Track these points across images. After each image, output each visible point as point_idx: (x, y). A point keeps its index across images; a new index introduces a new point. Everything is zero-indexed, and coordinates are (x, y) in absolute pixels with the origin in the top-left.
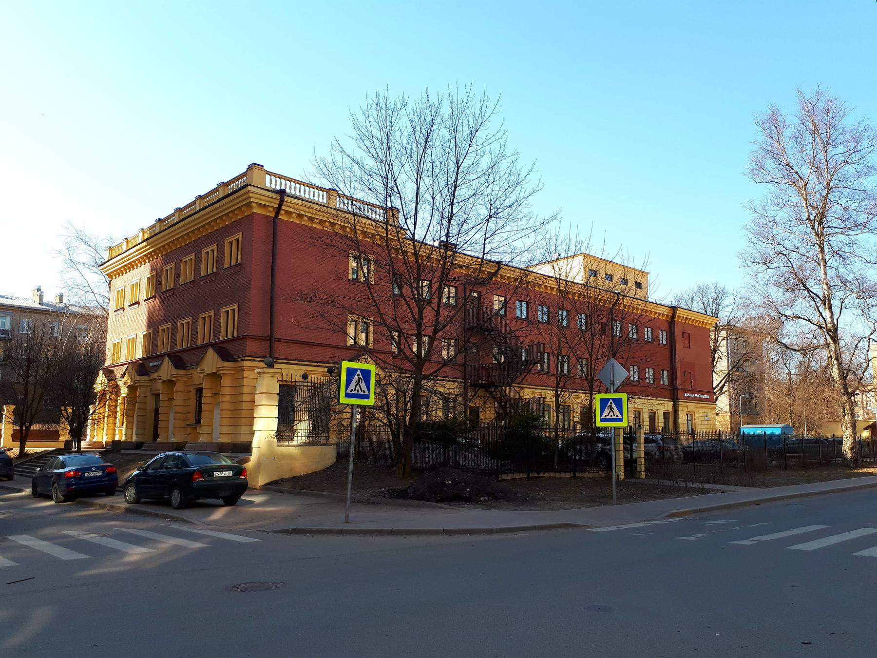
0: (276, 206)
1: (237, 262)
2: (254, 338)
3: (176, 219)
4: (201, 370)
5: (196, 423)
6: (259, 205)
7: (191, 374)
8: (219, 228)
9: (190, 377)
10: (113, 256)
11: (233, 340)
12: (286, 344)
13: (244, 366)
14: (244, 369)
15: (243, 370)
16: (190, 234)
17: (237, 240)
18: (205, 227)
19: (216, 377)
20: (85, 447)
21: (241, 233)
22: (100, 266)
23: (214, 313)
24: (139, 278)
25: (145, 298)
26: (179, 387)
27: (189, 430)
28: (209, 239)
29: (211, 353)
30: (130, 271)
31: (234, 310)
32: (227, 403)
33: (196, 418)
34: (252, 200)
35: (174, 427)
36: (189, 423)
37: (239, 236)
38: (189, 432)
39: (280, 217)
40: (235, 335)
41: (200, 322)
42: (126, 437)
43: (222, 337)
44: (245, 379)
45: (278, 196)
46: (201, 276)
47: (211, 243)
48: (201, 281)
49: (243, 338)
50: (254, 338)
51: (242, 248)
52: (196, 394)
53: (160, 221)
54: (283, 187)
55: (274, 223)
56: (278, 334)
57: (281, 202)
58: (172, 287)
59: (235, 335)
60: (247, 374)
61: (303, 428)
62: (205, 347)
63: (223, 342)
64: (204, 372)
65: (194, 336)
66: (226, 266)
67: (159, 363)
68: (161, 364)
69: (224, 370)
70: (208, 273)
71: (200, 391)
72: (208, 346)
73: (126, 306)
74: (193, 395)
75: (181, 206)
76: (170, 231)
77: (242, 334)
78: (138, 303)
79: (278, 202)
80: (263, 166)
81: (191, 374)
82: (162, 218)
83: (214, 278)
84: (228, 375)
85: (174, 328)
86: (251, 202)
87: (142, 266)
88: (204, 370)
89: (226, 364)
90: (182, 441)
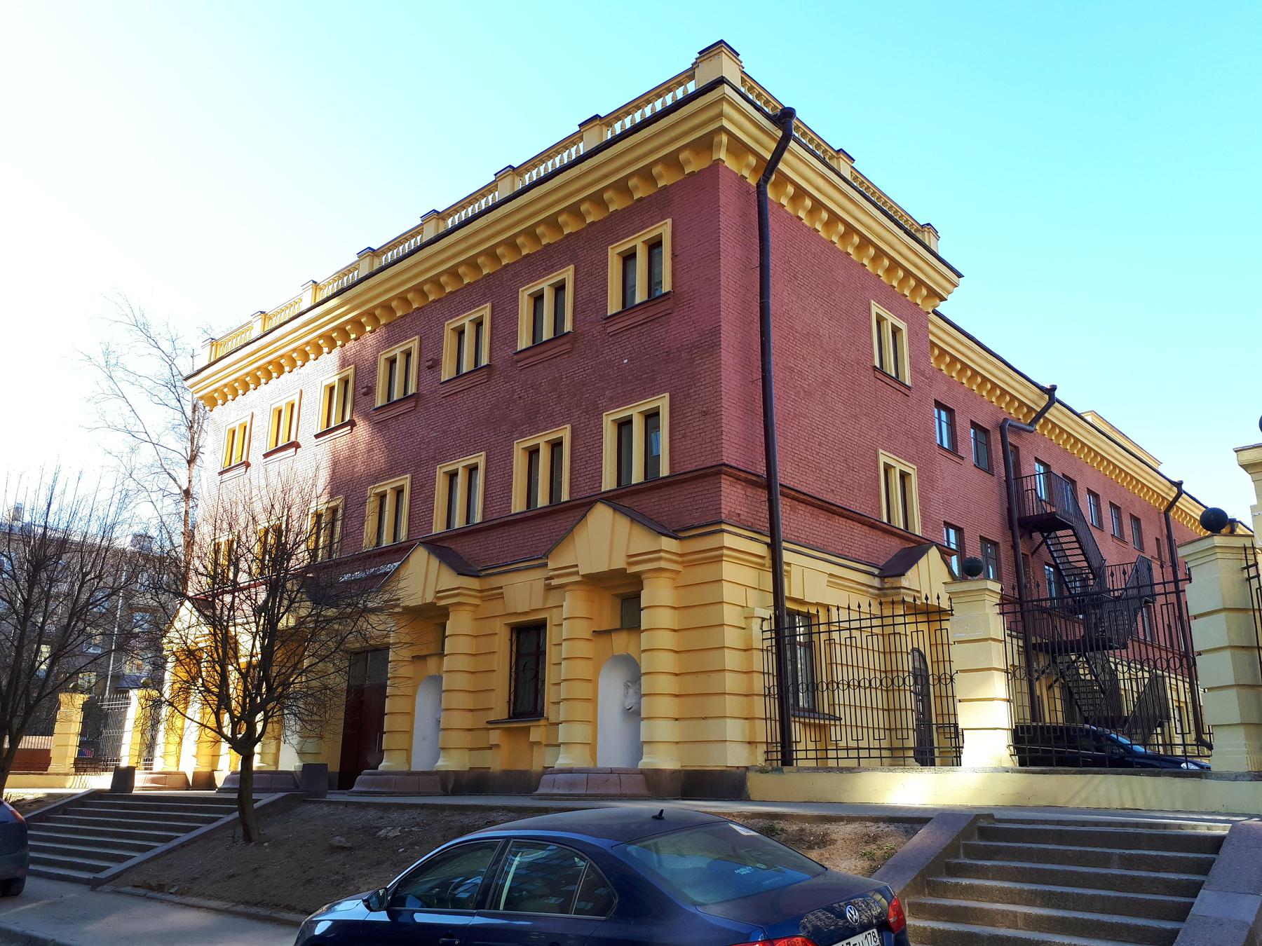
3: (429, 233)
5: (510, 718)
8: (539, 248)
9: (497, 595)
14: (722, 556)
15: (718, 560)
20: (141, 785)
21: (669, 221)
22: (186, 379)
23: (572, 433)
24: (298, 391)
25: (319, 432)
27: (495, 737)
29: (420, 558)
30: (235, 395)
36: (492, 716)
40: (478, 518)
41: (371, 506)
42: (262, 761)
49: (707, 475)
52: (511, 640)
53: (436, 215)
58: (412, 389)
59: (478, 518)
61: (898, 713)
64: (577, 573)
66: (524, 341)
69: (660, 559)
70: (333, 425)
73: (256, 458)
74: (502, 644)
76: (245, 353)
78: (296, 445)
80: (738, 55)
81: (501, 588)
82: (375, 248)
83: (568, 346)
87: (295, 370)
90: (467, 769)
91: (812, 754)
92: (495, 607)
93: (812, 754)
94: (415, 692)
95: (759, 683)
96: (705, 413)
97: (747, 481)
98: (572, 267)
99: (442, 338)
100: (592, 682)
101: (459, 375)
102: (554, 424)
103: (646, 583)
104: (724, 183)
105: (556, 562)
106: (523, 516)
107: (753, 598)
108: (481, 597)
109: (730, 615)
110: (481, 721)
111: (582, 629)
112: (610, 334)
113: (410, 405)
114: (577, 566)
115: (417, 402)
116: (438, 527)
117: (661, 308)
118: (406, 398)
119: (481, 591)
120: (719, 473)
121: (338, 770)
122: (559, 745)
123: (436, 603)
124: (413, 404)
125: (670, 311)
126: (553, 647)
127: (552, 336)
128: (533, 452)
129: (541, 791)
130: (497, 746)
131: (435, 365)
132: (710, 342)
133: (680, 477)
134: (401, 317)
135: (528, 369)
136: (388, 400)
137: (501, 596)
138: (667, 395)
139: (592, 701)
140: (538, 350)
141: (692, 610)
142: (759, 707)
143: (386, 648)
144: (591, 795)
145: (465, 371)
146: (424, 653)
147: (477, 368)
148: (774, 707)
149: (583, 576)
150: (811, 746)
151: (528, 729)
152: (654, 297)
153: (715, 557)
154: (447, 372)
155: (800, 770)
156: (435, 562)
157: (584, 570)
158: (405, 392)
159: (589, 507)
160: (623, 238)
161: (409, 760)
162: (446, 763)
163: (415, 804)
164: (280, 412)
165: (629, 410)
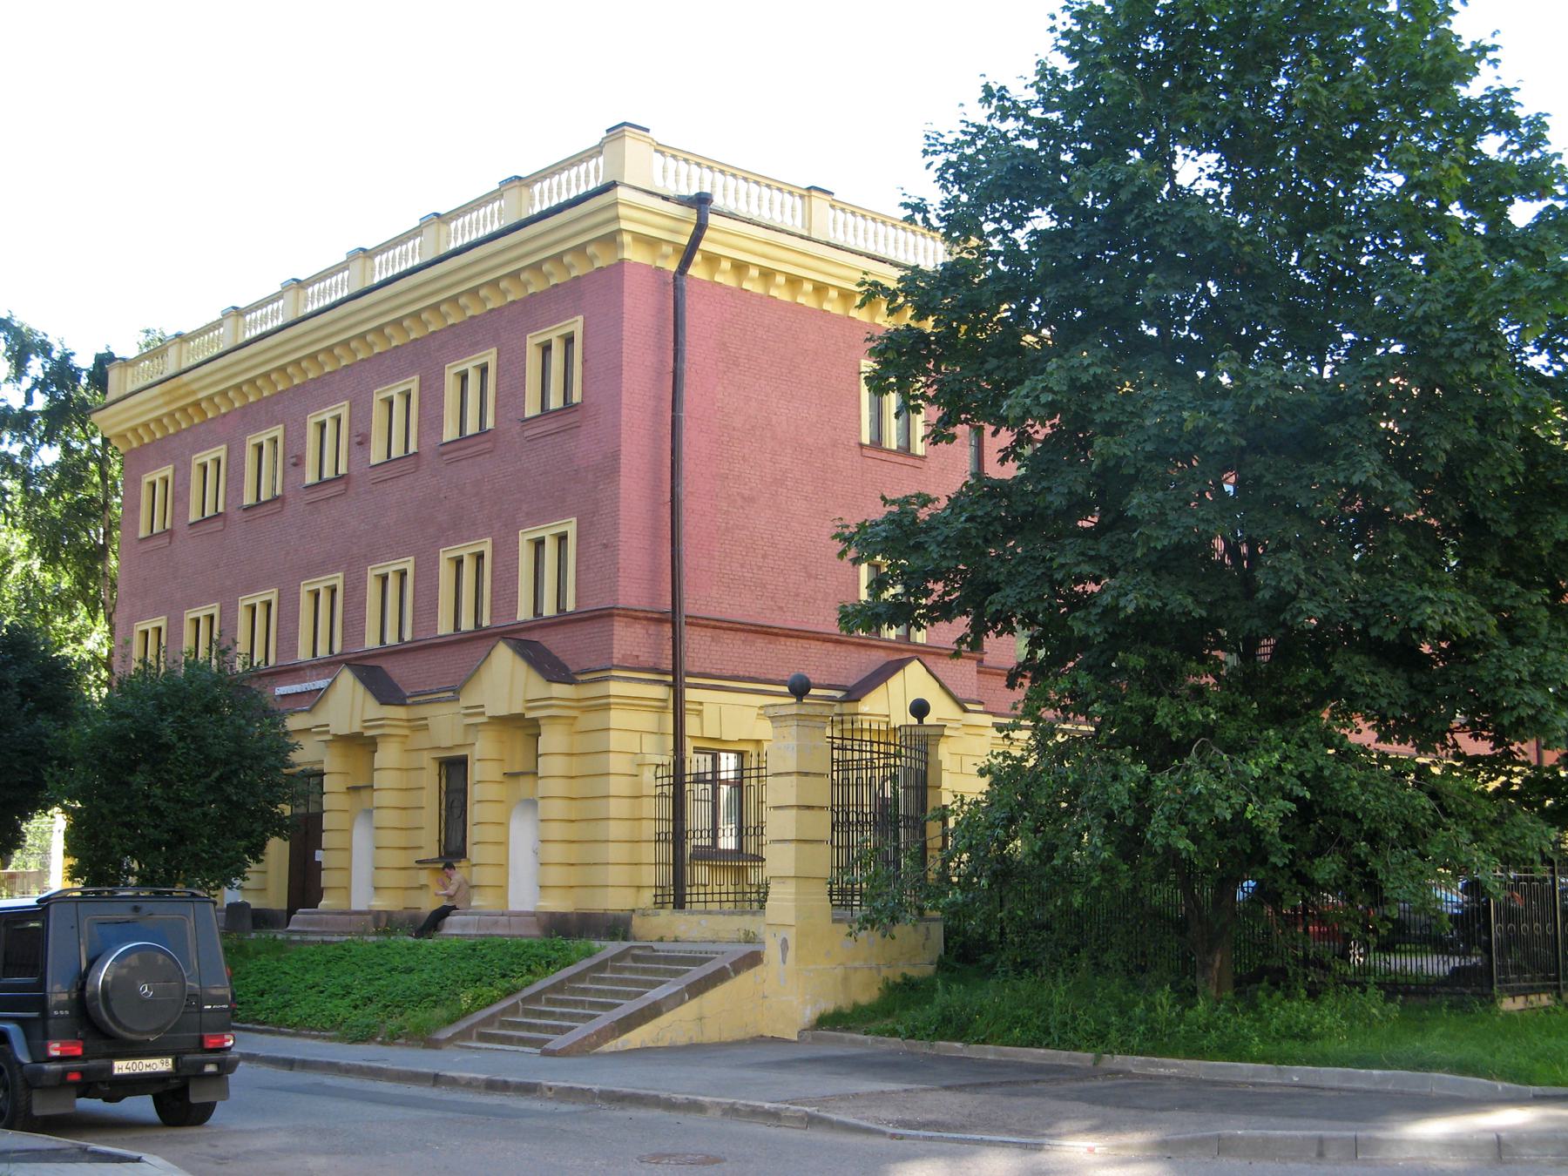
0: (685, 241)
1: (203, 515)
2: (632, 615)
4: (467, 708)
6: (640, 238)
7: (426, 719)
8: (465, 318)
9: (420, 726)
10: (185, 366)
11: (563, 619)
12: (709, 632)
13: (609, 696)
16: (290, 370)
17: (569, 340)
18: (478, 293)
19: (524, 727)
21: (580, 318)
26: (387, 755)
27: (424, 877)
28: (388, 365)
31: (562, 538)
32: (559, 802)
33: (440, 840)
34: (624, 225)
35: (265, 872)
37: (576, 325)
38: (423, 882)
39: (691, 271)
41: (373, 588)
43: (371, 642)
44: (612, 733)
45: (692, 215)
46: (445, 440)
47: (402, 374)
48: (443, 454)
49: (601, 617)
50: (632, 615)
51: (584, 361)
52: (440, 774)
54: (707, 189)
55: (676, 288)
56: (690, 606)
57: (701, 227)
58: (413, 448)
59: (407, 637)
60: (617, 718)
62: (482, 638)
63: (374, 655)
65: (427, 607)
66: (450, 433)
67: (322, 684)
68: (331, 685)
70: (206, 515)
71: (454, 769)
72: (340, 662)
74: (430, 780)
75: (186, 330)
77: (593, 604)
79: (691, 229)
80: (647, 130)
81: (426, 719)
83: (488, 445)
84: (563, 721)
85: (355, 590)
86: (620, 231)
88: (483, 706)
89: (560, 690)
91: (731, 897)
92: (421, 740)
93: (731, 897)
94: (508, 819)
95: (649, 830)
96: (606, 546)
97: (649, 619)
98: (494, 350)
99: (371, 410)
100: (503, 825)
101: (463, 437)
102: (476, 535)
103: (543, 729)
104: (630, 283)
105: (469, 698)
107: (649, 744)
108: (409, 728)
109: (617, 763)
110: (409, 859)
113: (340, 487)
115: (171, 538)
116: (524, 613)
117: (571, 418)
118: (407, 456)
119: (409, 720)
120: (611, 616)
124: (343, 487)
127: (477, 431)
128: (539, 544)
131: (298, 462)
132: (610, 467)
134: (330, 373)
136: (461, 434)
137: (426, 728)
138: (574, 520)
139: (503, 844)
140: (462, 444)
141: (589, 757)
142: (648, 852)
143: (321, 774)
145: (468, 433)
146: (360, 784)
147: (483, 432)
148: (667, 851)
149: (334, 735)
150: (731, 889)
152: (568, 406)
153: (603, 705)
154: (377, 455)
155: (692, 913)
156: (360, 688)
157: (491, 711)
158: (203, 515)
160: (541, 328)
161: (505, 897)
162: (380, 903)
164: (391, 404)
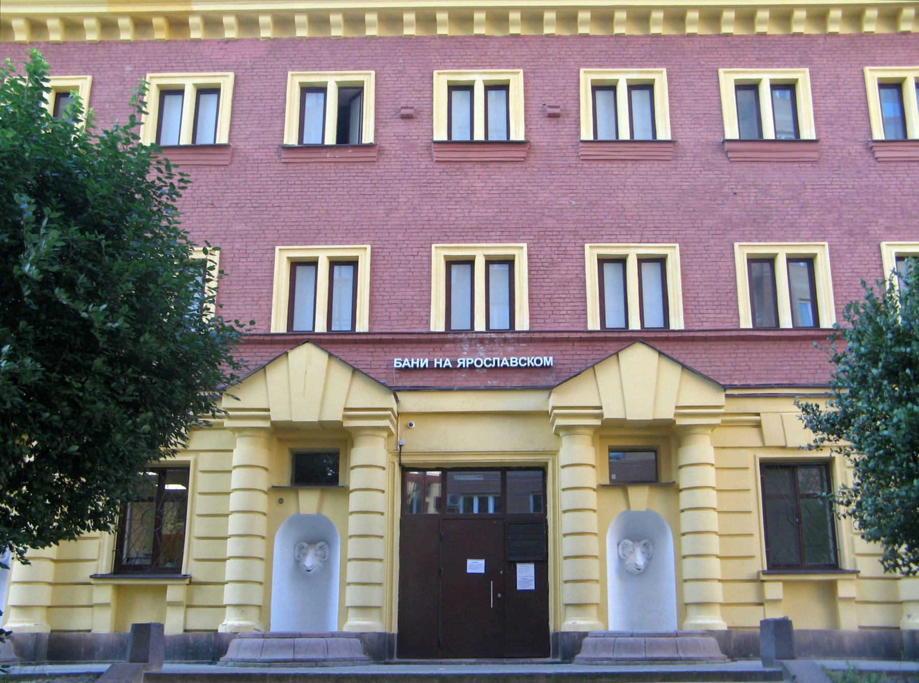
106: (679, 335)
111: (591, 477)
112: (731, 159)
114: (268, 410)
121: (395, 630)
122: (225, 606)
123: (674, 421)
125: (375, 159)
126: (198, 496)
129: (230, 654)
130: (779, 601)
133: (378, 337)
135: (745, 164)
144: (302, 661)
149: (272, 423)
151: (164, 588)
159: (629, 343)
163: (237, 674)
165: (316, 251)
